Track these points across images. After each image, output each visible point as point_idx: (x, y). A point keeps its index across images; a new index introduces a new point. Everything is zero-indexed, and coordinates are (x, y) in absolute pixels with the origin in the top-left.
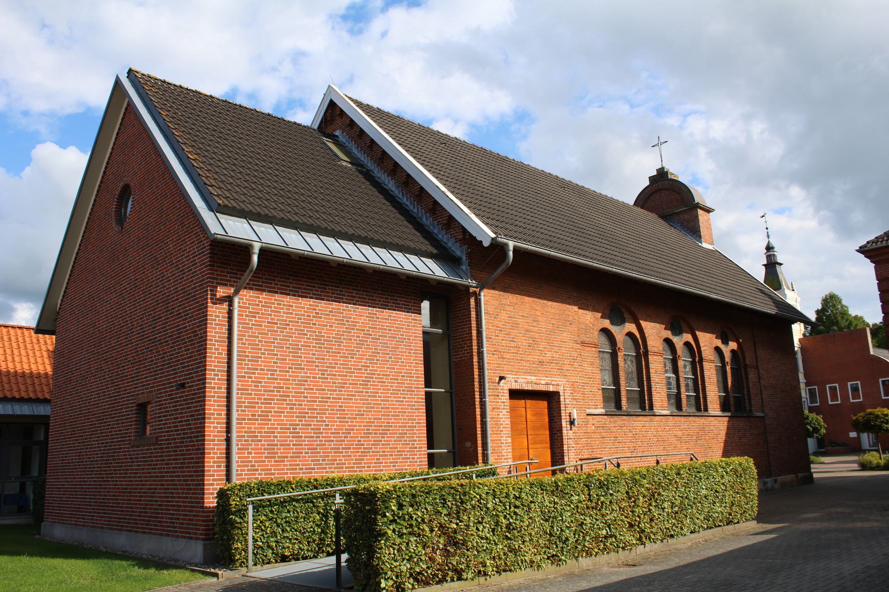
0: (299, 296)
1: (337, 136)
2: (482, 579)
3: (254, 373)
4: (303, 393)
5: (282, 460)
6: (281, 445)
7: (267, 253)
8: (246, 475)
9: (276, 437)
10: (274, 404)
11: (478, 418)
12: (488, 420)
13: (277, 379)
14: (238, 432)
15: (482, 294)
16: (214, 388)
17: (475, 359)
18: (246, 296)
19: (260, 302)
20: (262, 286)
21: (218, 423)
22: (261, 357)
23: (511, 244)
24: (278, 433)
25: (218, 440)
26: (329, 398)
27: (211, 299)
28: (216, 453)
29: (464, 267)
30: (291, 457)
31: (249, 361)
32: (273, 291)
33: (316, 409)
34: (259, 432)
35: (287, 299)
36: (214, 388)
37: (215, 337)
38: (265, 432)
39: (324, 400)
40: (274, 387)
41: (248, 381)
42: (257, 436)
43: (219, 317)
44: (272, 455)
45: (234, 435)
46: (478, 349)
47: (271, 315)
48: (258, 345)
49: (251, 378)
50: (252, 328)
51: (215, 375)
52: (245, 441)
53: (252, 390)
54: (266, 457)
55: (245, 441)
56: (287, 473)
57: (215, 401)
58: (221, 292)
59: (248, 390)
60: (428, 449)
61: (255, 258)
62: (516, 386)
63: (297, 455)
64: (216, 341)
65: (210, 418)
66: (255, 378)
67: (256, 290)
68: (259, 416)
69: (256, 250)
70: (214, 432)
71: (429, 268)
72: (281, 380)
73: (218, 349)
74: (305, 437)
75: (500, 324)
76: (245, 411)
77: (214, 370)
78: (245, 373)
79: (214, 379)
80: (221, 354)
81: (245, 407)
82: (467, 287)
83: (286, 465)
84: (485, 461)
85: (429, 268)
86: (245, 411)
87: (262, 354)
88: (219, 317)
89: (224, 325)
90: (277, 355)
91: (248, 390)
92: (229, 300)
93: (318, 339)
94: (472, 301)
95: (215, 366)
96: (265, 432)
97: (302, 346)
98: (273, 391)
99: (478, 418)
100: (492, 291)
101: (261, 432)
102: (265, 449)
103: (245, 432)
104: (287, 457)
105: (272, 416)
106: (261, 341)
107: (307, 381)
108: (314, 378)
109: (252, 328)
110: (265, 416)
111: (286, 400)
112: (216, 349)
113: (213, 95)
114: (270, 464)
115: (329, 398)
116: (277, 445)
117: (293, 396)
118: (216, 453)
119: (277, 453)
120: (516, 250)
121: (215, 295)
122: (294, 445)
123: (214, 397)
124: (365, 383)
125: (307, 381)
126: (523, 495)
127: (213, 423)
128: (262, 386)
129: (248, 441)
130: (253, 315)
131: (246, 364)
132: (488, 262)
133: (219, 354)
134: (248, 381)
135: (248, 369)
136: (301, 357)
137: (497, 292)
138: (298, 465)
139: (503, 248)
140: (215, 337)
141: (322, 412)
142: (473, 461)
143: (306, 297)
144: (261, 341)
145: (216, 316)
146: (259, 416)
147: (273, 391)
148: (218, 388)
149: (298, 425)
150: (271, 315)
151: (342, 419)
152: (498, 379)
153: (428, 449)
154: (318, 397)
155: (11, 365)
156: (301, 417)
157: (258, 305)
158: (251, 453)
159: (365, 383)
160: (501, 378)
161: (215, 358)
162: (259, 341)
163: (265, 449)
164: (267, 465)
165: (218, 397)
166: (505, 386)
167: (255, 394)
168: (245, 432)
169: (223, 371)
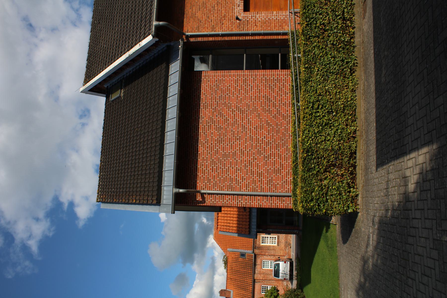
0: (198, 153)
1: (108, 87)
2: (358, 133)
3: (238, 180)
4: (248, 151)
5: (282, 165)
6: (274, 166)
7: (178, 183)
8: (288, 186)
9: (270, 168)
10: (253, 169)
11: (261, 37)
12: (262, 32)
13: (241, 167)
14: (267, 192)
15: (187, 34)
16: (246, 203)
17: (226, 39)
18: (200, 184)
19: (202, 177)
20: (194, 175)
21: (263, 201)
22: (230, 176)
23: (155, 23)
24: (268, 167)
25: (271, 201)
26: (250, 135)
27: (203, 203)
28: (278, 202)
29: (172, 44)
30: (281, 160)
31: (232, 183)
32: (196, 169)
33: (256, 144)
34: (268, 178)
35: (200, 160)
36: (246, 203)
37: (221, 202)
38: (268, 175)
39: (251, 138)
40: (245, 169)
41: (242, 184)
42: (270, 179)
43: (211, 200)
44: (279, 171)
45: (269, 194)
46: (220, 36)
47: (209, 170)
48: (224, 178)
49: (240, 182)
50: (216, 181)
51: (240, 202)
52: (272, 186)
53: (247, 182)
54: (280, 175)
55: (272, 186)
56: (289, 163)
57: (252, 202)
58: (199, 198)
59: (247, 184)
60: (278, 69)
61: (181, 191)
62: (242, 7)
63: (280, 156)
64: (223, 201)
65: (261, 205)
66: (240, 180)
67: (196, 178)
68: (259, 178)
69: (177, 190)
70: (267, 203)
71: (175, 68)
72: (241, 165)
73: (227, 200)
74: (271, 151)
75: (205, 18)
76: (257, 186)
77: (238, 202)
78: (238, 185)
79: (242, 202)
80: (229, 198)
81: (255, 186)
82: (184, 43)
83: (285, 163)
84: (285, 34)
85: (175, 68)
86: (257, 186)
87: (228, 176)
88: (211, 200)
89: (215, 196)
90: (229, 167)
91: (247, 184)
92: (202, 195)
93: (219, 142)
94: (192, 40)
95: (235, 202)
96: (268, 175)
97: (223, 152)
98: (247, 169)
99: (261, 37)
100: (185, 23)
101: (268, 177)
102: (276, 175)
103: (268, 186)
104: (281, 162)
105: (260, 171)
106: (222, 176)
107: (242, 149)
108: (240, 145)
109: (216, 181)
110: (260, 175)
111: (252, 162)
112: (227, 201)
113: (100, 160)
114: (284, 173)
115: (250, 135)
116: (274, 168)
117: (250, 158)
118: (278, 202)
119: (278, 168)
120: (158, 19)
121: (201, 201)
122: (274, 158)
123: (250, 203)
124: (243, 112)
125: (242, 149)
126: (312, 101)
127: (263, 203)
128: (245, 176)
129: (272, 185)
130: (209, 181)
131: (234, 185)
132: (169, 35)
133: (229, 200)
134: (242, 184)
135: (236, 184)
136: (229, 152)
137: (185, 19)
138: (285, 155)
139: (157, 27)
140: (221, 202)
141: (257, 140)
142: (287, 41)
143: (198, 148)
144: (222, 176)
145: (211, 201)
146: (259, 178)
147: (247, 169)
148: (246, 200)
149: (264, 155)
150: (209, 170)
151: (261, 127)
152: (238, 21)
153: (278, 69)
154: (250, 142)
155: (235, 219)
156: (259, 153)
157: (204, 177)
158: (278, 183)
159: (243, 112)
160: (237, 18)
161: (231, 202)
162: (222, 177)
163: (276, 175)
164: (284, 174)
165: (250, 201)
166: (242, 15)
167: (249, 180)
168: (268, 186)
169: (238, 197)
